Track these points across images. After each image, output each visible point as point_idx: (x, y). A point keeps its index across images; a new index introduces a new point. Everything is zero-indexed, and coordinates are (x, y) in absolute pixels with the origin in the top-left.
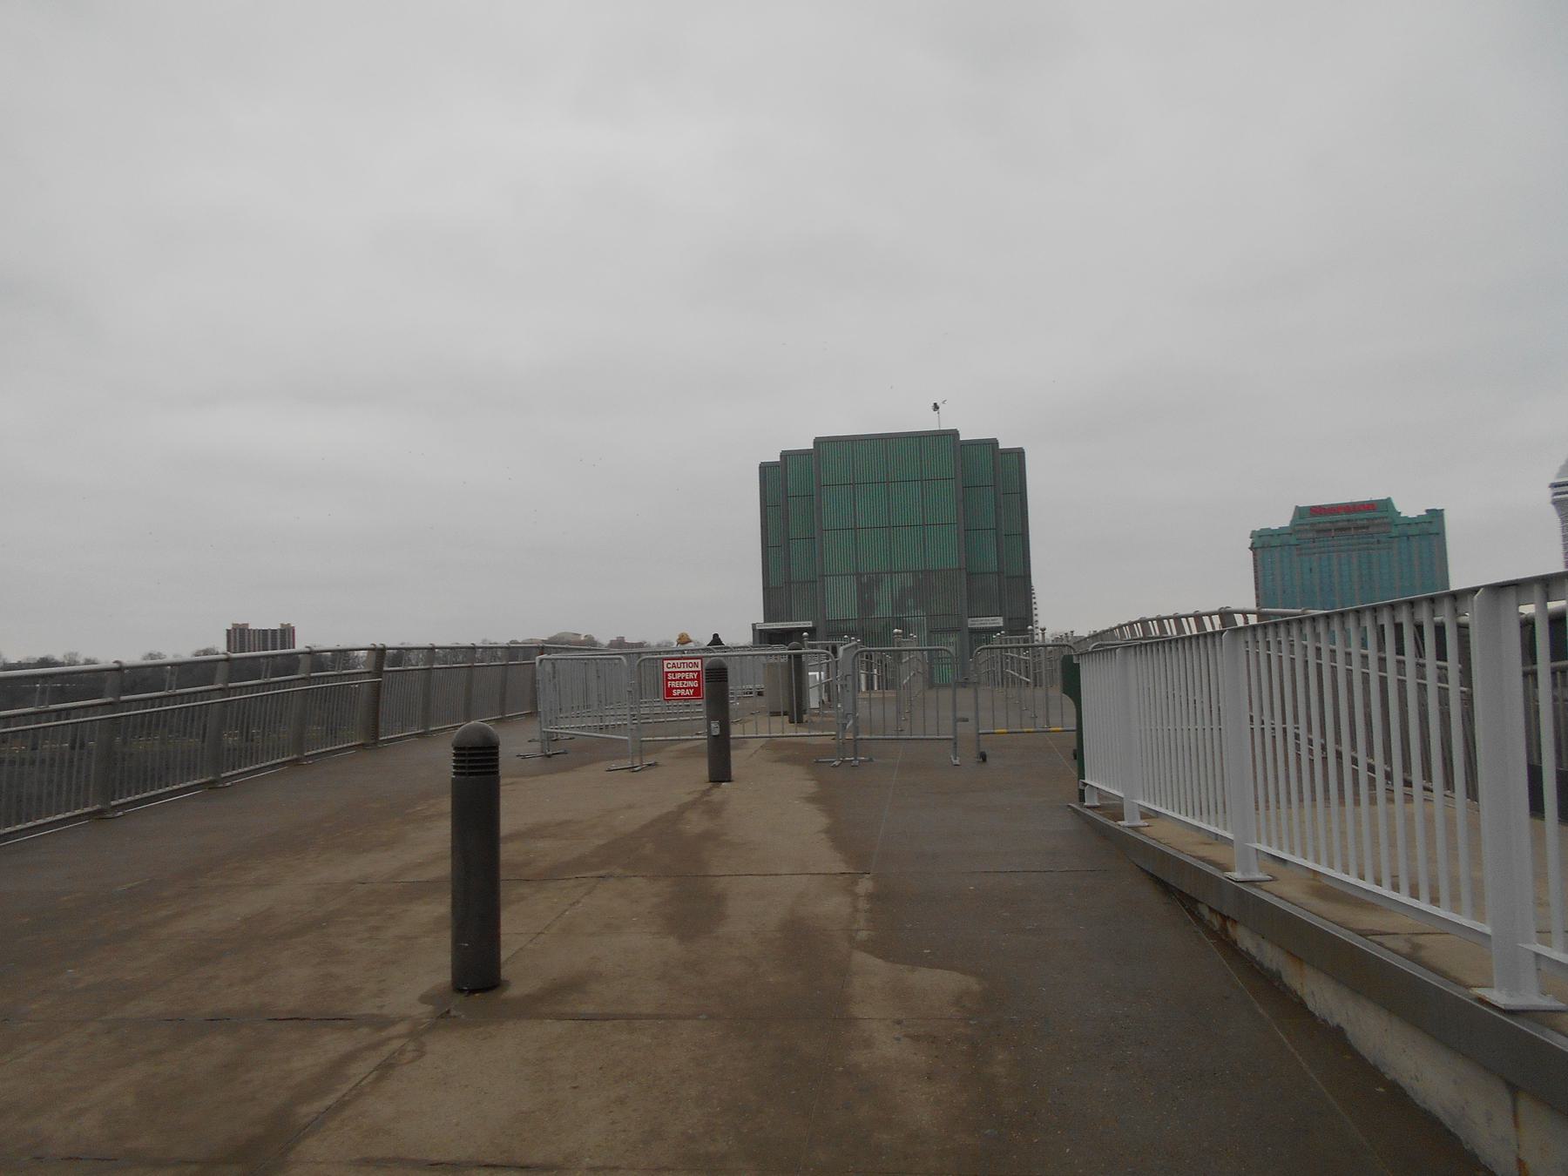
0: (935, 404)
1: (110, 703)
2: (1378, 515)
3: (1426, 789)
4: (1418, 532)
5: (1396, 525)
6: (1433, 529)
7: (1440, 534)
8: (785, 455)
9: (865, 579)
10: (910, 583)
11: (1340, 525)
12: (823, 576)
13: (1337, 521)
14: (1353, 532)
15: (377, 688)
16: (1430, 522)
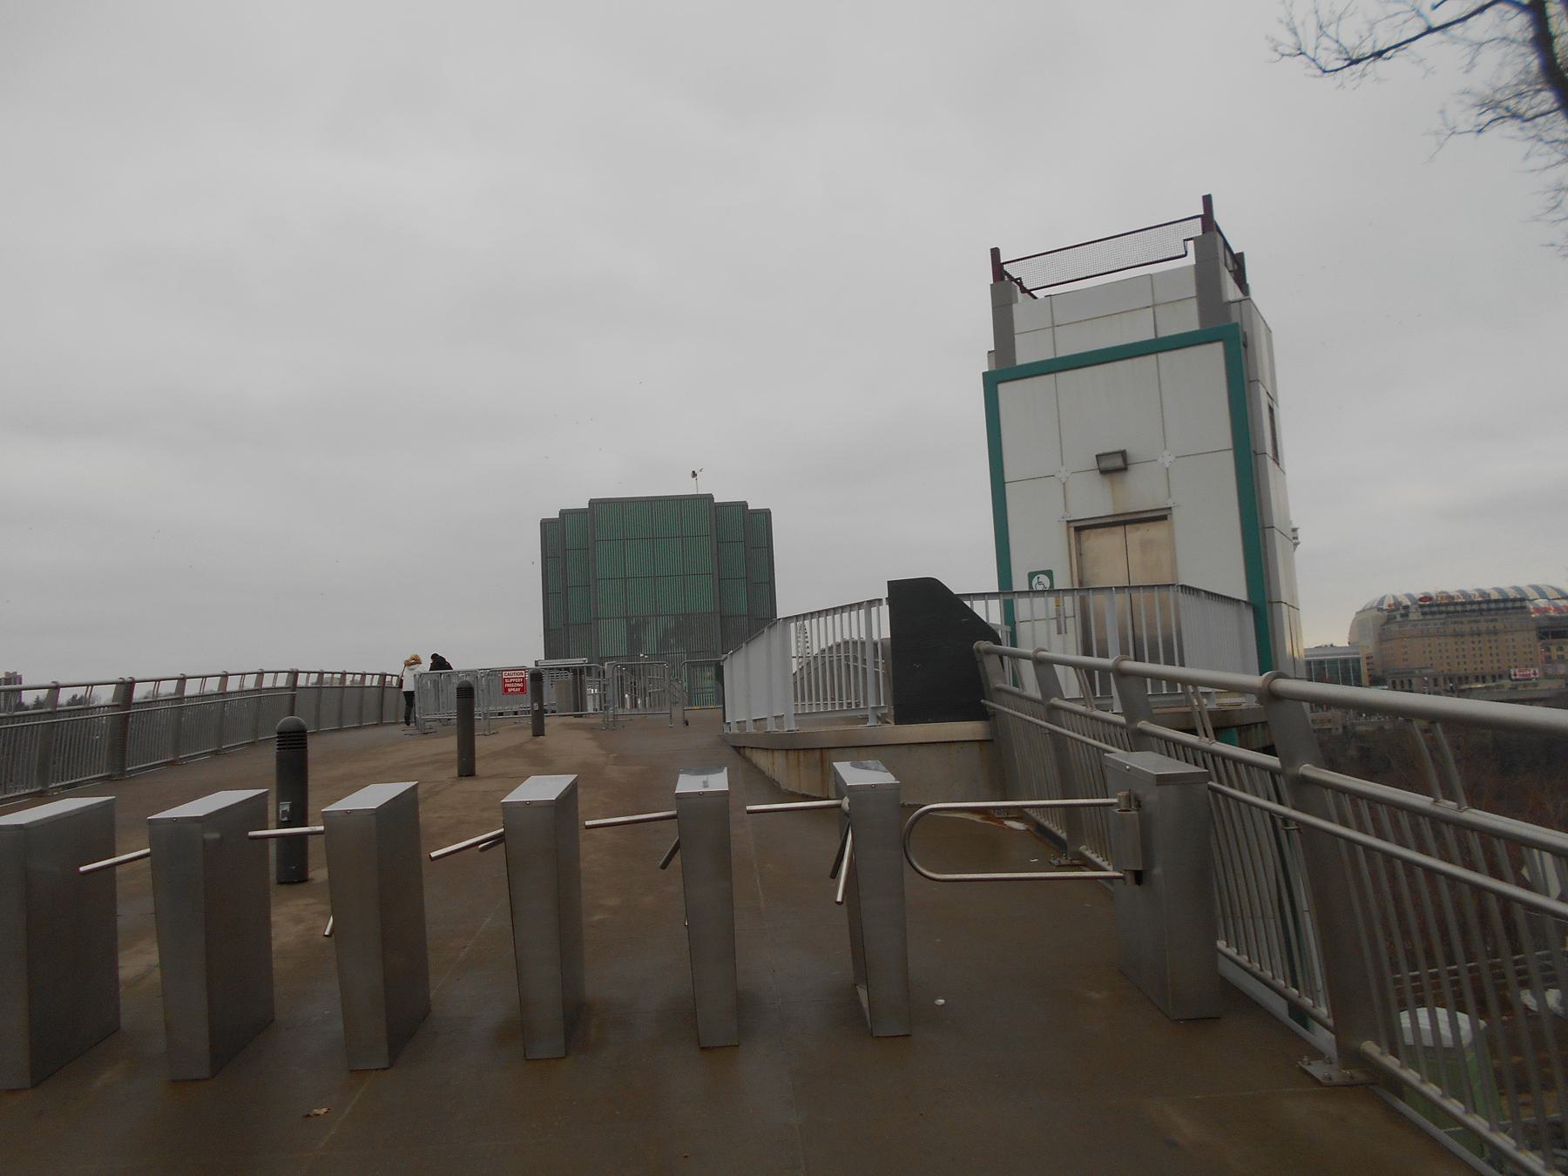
0: (694, 472)
1: (49, 713)
8: (563, 513)
10: (672, 624)
12: (598, 619)
15: (293, 697)
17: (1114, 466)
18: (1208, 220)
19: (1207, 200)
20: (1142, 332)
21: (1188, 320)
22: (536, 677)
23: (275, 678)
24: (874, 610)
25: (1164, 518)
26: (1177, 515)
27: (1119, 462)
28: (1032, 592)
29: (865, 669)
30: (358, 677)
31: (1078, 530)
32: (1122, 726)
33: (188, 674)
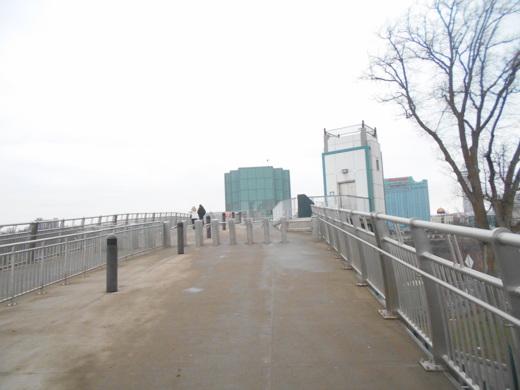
2: (408, 181)
3: (458, 283)
4: (420, 187)
5: (414, 185)
6: (424, 186)
7: (426, 187)
8: (231, 172)
9: (251, 202)
10: (261, 203)
11: (397, 184)
13: (396, 183)
14: (401, 186)
16: (423, 184)
17: (345, 172)
18: (363, 125)
19: (363, 121)
20: (351, 146)
21: (359, 144)
22: (224, 215)
23: (133, 216)
24: (295, 199)
25: (354, 182)
26: (356, 181)
27: (346, 171)
28: (330, 196)
29: (463, 280)
30: (159, 214)
31: (339, 184)
32: (413, 253)
33: (129, 213)
